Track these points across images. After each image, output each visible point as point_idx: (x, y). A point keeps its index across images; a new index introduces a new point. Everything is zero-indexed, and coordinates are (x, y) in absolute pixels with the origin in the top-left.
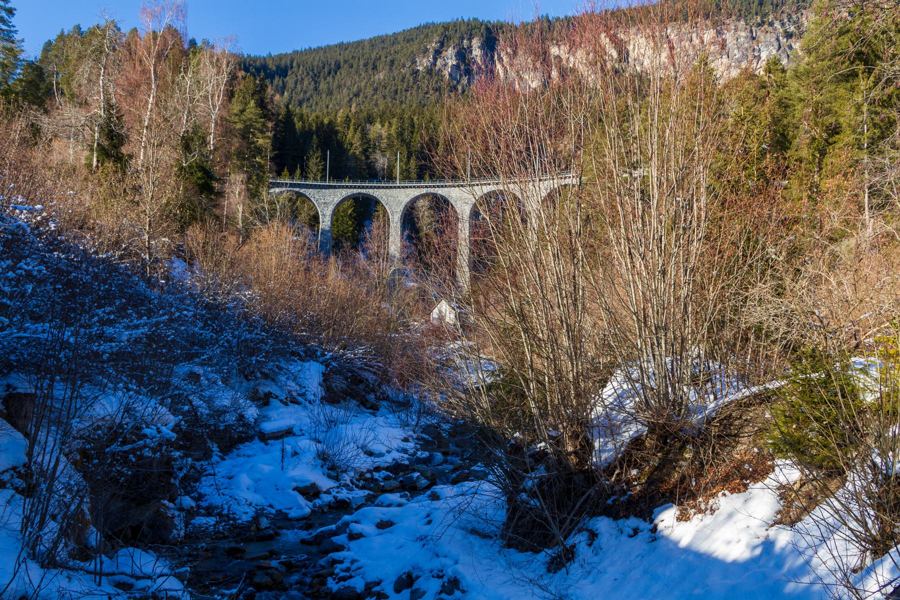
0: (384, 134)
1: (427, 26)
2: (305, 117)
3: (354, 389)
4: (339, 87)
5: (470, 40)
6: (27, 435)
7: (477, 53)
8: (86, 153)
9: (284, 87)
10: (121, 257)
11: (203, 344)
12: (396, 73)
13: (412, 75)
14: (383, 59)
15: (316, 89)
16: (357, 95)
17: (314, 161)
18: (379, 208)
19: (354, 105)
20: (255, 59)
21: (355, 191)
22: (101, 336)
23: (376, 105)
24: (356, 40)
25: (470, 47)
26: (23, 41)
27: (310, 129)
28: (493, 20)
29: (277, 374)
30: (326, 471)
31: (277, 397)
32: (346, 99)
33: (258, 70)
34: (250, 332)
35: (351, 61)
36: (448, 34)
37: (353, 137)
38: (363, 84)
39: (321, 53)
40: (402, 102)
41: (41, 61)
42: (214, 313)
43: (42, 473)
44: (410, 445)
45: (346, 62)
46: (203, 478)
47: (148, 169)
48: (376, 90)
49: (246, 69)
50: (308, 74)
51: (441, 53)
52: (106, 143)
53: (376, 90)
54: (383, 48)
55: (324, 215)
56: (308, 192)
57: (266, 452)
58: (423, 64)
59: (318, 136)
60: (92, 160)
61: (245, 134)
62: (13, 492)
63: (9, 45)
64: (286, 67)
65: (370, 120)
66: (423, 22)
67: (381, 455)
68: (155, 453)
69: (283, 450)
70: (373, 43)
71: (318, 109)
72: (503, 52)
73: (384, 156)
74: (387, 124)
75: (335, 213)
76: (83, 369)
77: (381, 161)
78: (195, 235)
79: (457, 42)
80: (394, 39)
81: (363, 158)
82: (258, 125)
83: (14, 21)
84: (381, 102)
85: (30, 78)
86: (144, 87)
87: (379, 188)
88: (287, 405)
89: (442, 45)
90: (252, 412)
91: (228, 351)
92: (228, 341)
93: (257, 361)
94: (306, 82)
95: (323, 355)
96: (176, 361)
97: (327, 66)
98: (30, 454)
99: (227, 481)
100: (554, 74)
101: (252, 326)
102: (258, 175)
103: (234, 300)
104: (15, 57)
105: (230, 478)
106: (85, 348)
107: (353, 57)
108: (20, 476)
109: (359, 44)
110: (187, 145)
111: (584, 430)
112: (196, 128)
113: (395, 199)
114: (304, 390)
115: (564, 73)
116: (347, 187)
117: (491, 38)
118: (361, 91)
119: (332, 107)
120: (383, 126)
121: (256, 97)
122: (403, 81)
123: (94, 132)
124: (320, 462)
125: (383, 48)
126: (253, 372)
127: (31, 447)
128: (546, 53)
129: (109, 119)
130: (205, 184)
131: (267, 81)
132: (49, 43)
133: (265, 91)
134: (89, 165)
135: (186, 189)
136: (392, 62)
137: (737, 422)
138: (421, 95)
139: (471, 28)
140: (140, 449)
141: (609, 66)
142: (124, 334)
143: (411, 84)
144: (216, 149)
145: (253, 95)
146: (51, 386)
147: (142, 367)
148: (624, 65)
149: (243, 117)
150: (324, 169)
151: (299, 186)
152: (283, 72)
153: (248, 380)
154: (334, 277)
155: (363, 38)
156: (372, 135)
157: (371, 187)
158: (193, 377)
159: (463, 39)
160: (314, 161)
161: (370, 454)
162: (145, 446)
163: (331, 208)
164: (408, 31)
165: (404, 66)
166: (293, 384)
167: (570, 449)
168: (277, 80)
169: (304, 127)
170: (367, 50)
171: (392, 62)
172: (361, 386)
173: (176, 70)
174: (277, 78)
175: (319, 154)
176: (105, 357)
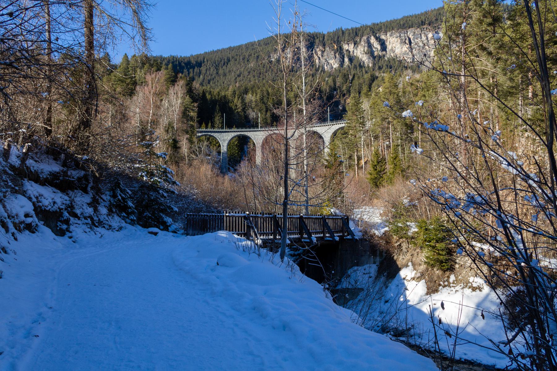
2: (212, 93)
4: (230, 71)
9: (200, 73)
14: (253, 55)
15: (217, 73)
16: (239, 76)
17: (218, 118)
20: (184, 58)
23: (250, 81)
24: (238, 45)
32: (234, 78)
35: (235, 57)
37: (237, 102)
38: (242, 69)
45: (233, 57)
48: (249, 72)
50: (213, 65)
53: (249, 72)
54: (253, 49)
55: (223, 146)
56: (215, 135)
64: (201, 62)
65: (246, 92)
72: (318, 50)
74: (255, 94)
75: (229, 144)
77: (252, 115)
84: (252, 79)
87: (250, 131)
94: (212, 70)
97: (222, 60)
100: (346, 60)
102: (191, 131)
107: (237, 55)
109: (240, 47)
113: (258, 136)
115: (351, 60)
116: (234, 131)
118: (241, 73)
119: (225, 87)
120: (252, 95)
122: (264, 67)
125: (253, 49)
128: (341, 49)
136: (258, 57)
138: (273, 75)
141: (376, 54)
148: (384, 53)
151: (211, 132)
152: (199, 64)
154: (227, 183)
156: (247, 101)
157: (246, 131)
163: (227, 142)
168: (196, 70)
169: (212, 98)
170: (244, 51)
171: (258, 57)
174: (196, 68)
175: (220, 114)
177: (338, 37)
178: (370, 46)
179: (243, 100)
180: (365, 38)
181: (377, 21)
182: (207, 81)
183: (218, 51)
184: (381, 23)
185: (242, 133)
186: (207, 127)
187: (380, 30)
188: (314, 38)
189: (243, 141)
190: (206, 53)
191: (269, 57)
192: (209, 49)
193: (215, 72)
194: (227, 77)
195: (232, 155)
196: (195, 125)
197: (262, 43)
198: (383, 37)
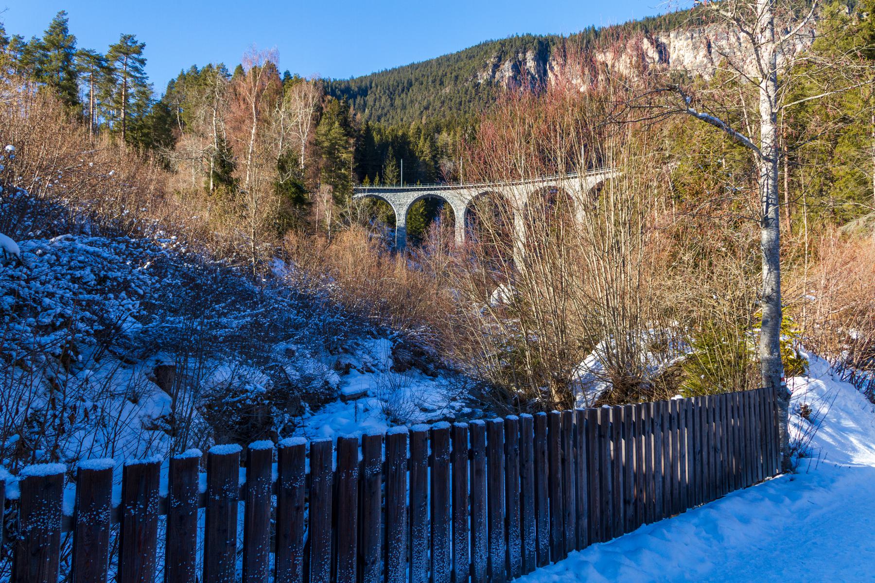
0: (450, 141)
1: (486, 44)
2: (383, 131)
3: (415, 360)
5: (524, 53)
6: (171, 395)
7: (531, 64)
8: (205, 179)
9: (365, 105)
10: (234, 262)
11: (297, 327)
12: (460, 87)
13: (474, 87)
14: (449, 75)
16: (427, 108)
17: (390, 168)
18: (446, 206)
19: (424, 117)
21: (425, 193)
22: (218, 325)
23: (444, 116)
25: (525, 59)
26: (152, 84)
27: (387, 141)
28: (545, 34)
29: (355, 349)
30: (390, 423)
31: (355, 367)
32: (418, 112)
33: (343, 92)
34: (333, 317)
36: (506, 49)
37: (424, 145)
38: (432, 98)
39: (396, 74)
40: (465, 112)
41: (167, 97)
42: (305, 303)
43: (182, 420)
44: (457, 405)
46: (297, 429)
47: (251, 190)
48: (443, 103)
49: (333, 93)
50: (385, 92)
51: (499, 66)
52: (219, 171)
53: (443, 103)
57: (345, 409)
58: (483, 77)
59: (393, 148)
60: (209, 184)
61: (331, 152)
62: (163, 432)
63: (142, 89)
64: (366, 87)
65: (438, 130)
66: (483, 40)
67: (433, 410)
68: (253, 401)
69: (356, 407)
70: (440, 61)
71: (394, 123)
73: (450, 160)
74: (452, 133)
75: (409, 212)
76: (207, 348)
78: (291, 238)
79: (513, 55)
80: (458, 57)
81: (432, 163)
82: (342, 143)
83: (145, 69)
84: (448, 113)
85: (159, 115)
86: (247, 121)
87: (445, 189)
88: (363, 373)
89: (500, 59)
90: (334, 378)
91: (319, 332)
92: (316, 324)
93: (338, 339)
94: (383, 100)
95: (392, 333)
96: (275, 340)
97: (400, 84)
98: (173, 407)
99: (315, 431)
101: (334, 311)
102: (342, 184)
103: (321, 291)
104: (148, 99)
105: (317, 429)
106: (207, 333)
107: (423, 75)
108: (167, 421)
109: (428, 63)
110: (282, 167)
111: (566, 387)
112: (289, 152)
113: (457, 199)
114: (376, 362)
116: (418, 190)
117: (543, 49)
119: (405, 121)
120: (449, 134)
121: (341, 117)
122: (466, 93)
123: (210, 161)
124: (384, 416)
125: (448, 66)
126: (336, 348)
127: (174, 401)
129: (221, 151)
130: (297, 197)
131: (351, 101)
132: (172, 82)
133: (348, 111)
134: (207, 188)
135: (283, 203)
136: (457, 77)
137: (676, 379)
139: (525, 43)
140: (245, 400)
142: (234, 322)
143: (473, 96)
144: (306, 166)
145: (338, 115)
146: (186, 360)
147: (249, 347)
148: (665, 65)
149: (330, 137)
150: (399, 175)
152: (363, 92)
153: (333, 355)
154: (400, 270)
155: (431, 58)
157: (438, 189)
158: (289, 353)
159: (518, 53)
160: (390, 168)
161: (425, 410)
162: (247, 398)
163: (405, 208)
164: (470, 49)
165: (467, 80)
166: (367, 357)
167: (557, 400)
168: (359, 100)
169: (381, 139)
170: (434, 69)
171: (457, 77)
172: (423, 358)
173: (272, 105)
174: (359, 98)
176: (221, 339)
177: (588, 42)
178: (642, 56)
179: (433, 143)
180: (633, 41)
181: (653, 14)
182: (376, 118)
183: (394, 70)
184: (659, 17)
185: (432, 192)
186: (372, 183)
187: (658, 27)
188: (548, 45)
189: (433, 208)
190: (374, 74)
191: (475, 76)
192: (378, 68)
193: (388, 104)
194: (407, 112)
195: (415, 231)
196: (351, 175)
197: (463, 56)
198: (663, 40)
